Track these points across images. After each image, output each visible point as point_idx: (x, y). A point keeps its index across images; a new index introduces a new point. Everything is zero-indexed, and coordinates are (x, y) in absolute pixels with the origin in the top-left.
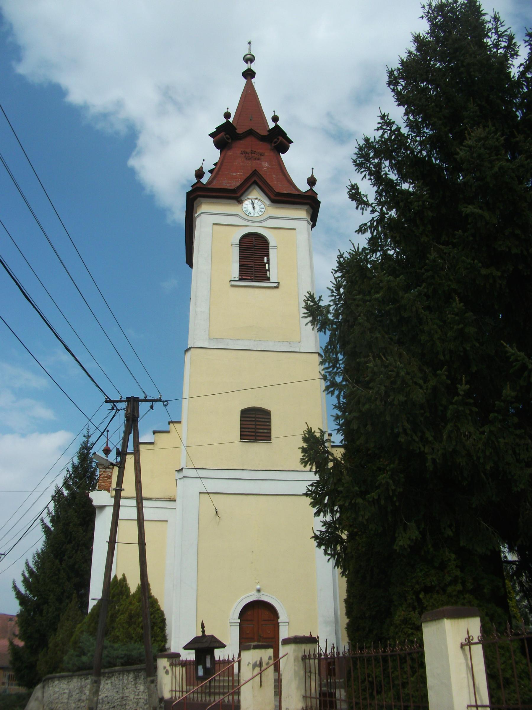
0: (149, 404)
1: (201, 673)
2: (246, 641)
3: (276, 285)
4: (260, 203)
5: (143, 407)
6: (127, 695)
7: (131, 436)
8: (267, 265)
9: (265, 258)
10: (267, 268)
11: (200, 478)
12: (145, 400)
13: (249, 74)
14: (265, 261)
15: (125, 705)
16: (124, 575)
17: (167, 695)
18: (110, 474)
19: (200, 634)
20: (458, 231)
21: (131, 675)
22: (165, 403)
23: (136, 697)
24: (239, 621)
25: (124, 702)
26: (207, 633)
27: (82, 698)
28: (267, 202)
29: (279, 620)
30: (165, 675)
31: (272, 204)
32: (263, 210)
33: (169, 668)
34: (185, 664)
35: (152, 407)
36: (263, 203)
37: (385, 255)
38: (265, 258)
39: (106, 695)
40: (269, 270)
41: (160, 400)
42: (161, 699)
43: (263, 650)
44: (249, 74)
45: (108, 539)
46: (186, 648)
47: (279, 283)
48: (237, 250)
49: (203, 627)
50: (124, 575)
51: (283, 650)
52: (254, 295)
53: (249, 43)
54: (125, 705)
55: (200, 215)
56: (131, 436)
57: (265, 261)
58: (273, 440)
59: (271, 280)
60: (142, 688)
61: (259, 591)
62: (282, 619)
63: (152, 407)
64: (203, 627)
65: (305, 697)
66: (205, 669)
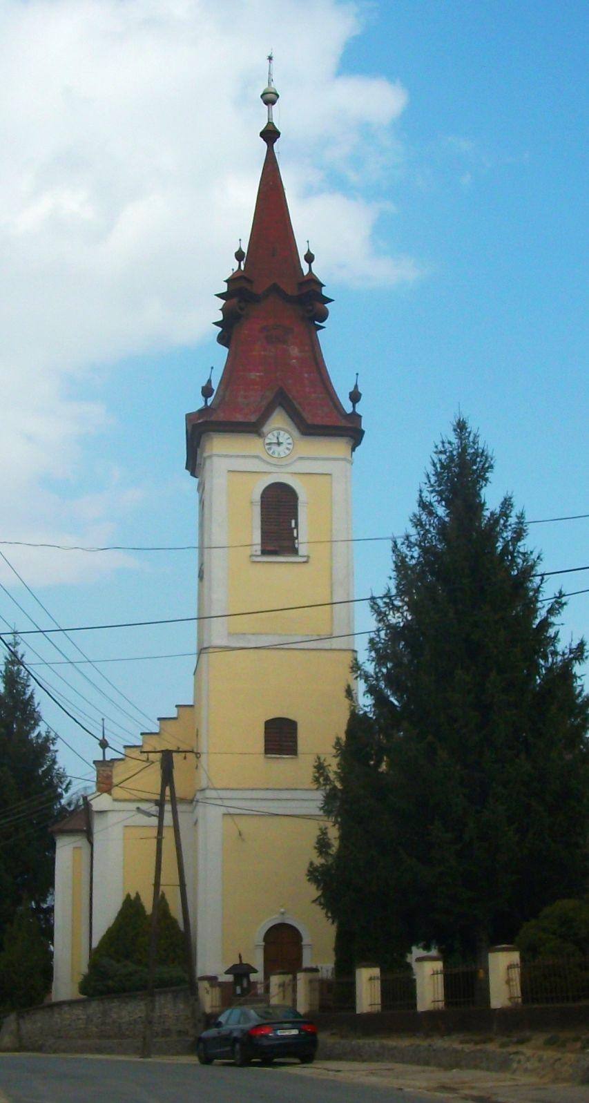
0: (183, 754)
1: (239, 990)
3: (304, 559)
4: (287, 436)
5: (177, 758)
6: (166, 1013)
7: (168, 789)
8: (295, 531)
9: (293, 522)
10: (295, 535)
11: (221, 799)
13: (270, 135)
14: (293, 525)
15: (164, 1022)
16: (137, 894)
17: (208, 1010)
19: (238, 962)
20: (497, 548)
21: (170, 996)
22: (198, 755)
23: (176, 1014)
25: (162, 1020)
26: (244, 962)
27: (107, 1021)
28: (296, 433)
29: (303, 943)
34: (221, 985)
35: (185, 758)
37: (407, 611)
38: (293, 522)
39: (139, 1016)
40: (297, 538)
41: (192, 752)
45: (153, 882)
47: (308, 557)
48: (257, 510)
49: (240, 957)
50: (137, 894)
51: (300, 976)
53: (270, 58)
54: (164, 1022)
56: (168, 789)
57: (293, 525)
60: (182, 1006)
61: (283, 914)
62: (306, 940)
63: (185, 758)
64: (240, 957)
65: (311, 1005)
66: (243, 989)
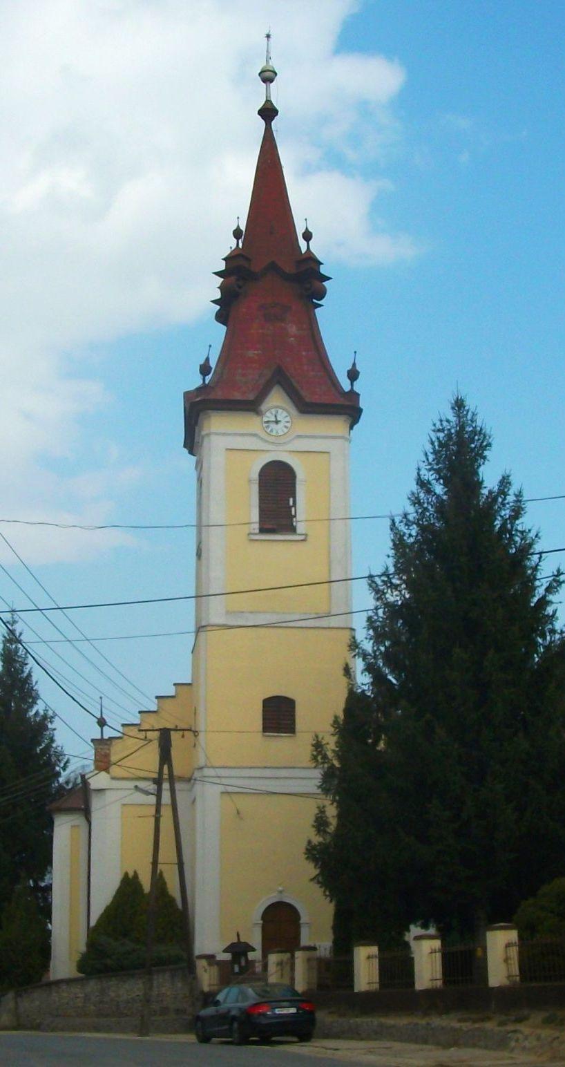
0: (181, 733)
1: (237, 969)
2: (269, 944)
3: (302, 538)
4: (285, 414)
5: (175, 736)
6: (164, 992)
7: (166, 767)
8: (293, 509)
9: (291, 500)
12: (176, 730)
13: (268, 113)
14: (291, 503)
15: (162, 1000)
16: (135, 872)
18: (108, 751)
19: (236, 941)
22: (197, 734)
24: (261, 922)
26: (242, 940)
28: (294, 411)
29: (301, 921)
30: (204, 973)
31: (300, 414)
32: (288, 425)
33: (207, 967)
35: (183, 736)
36: (288, 412)
37: (405, 589)
38: (291, 500)
40: (295, 516)
41: (190, 730)
42: (202, 992)
43: (283, 954)
44: (268, 113)
45: (151, 860)
46: (225, 951)
50: (135, 872)
51: (298, 954)
52: (278, 554)
53: (268, 36)
55: (208, 435)
57: (291, 503)
58: (298, 734)
59: (299, 531)
61: (281, 892)
62: (304, 919)
63: (183, 736)
66: (241, 967)
